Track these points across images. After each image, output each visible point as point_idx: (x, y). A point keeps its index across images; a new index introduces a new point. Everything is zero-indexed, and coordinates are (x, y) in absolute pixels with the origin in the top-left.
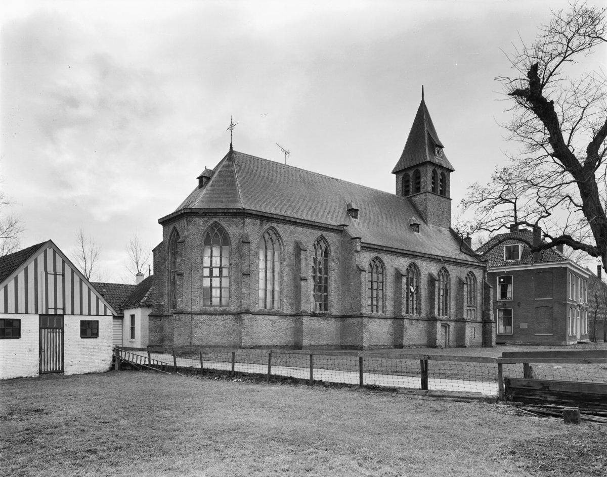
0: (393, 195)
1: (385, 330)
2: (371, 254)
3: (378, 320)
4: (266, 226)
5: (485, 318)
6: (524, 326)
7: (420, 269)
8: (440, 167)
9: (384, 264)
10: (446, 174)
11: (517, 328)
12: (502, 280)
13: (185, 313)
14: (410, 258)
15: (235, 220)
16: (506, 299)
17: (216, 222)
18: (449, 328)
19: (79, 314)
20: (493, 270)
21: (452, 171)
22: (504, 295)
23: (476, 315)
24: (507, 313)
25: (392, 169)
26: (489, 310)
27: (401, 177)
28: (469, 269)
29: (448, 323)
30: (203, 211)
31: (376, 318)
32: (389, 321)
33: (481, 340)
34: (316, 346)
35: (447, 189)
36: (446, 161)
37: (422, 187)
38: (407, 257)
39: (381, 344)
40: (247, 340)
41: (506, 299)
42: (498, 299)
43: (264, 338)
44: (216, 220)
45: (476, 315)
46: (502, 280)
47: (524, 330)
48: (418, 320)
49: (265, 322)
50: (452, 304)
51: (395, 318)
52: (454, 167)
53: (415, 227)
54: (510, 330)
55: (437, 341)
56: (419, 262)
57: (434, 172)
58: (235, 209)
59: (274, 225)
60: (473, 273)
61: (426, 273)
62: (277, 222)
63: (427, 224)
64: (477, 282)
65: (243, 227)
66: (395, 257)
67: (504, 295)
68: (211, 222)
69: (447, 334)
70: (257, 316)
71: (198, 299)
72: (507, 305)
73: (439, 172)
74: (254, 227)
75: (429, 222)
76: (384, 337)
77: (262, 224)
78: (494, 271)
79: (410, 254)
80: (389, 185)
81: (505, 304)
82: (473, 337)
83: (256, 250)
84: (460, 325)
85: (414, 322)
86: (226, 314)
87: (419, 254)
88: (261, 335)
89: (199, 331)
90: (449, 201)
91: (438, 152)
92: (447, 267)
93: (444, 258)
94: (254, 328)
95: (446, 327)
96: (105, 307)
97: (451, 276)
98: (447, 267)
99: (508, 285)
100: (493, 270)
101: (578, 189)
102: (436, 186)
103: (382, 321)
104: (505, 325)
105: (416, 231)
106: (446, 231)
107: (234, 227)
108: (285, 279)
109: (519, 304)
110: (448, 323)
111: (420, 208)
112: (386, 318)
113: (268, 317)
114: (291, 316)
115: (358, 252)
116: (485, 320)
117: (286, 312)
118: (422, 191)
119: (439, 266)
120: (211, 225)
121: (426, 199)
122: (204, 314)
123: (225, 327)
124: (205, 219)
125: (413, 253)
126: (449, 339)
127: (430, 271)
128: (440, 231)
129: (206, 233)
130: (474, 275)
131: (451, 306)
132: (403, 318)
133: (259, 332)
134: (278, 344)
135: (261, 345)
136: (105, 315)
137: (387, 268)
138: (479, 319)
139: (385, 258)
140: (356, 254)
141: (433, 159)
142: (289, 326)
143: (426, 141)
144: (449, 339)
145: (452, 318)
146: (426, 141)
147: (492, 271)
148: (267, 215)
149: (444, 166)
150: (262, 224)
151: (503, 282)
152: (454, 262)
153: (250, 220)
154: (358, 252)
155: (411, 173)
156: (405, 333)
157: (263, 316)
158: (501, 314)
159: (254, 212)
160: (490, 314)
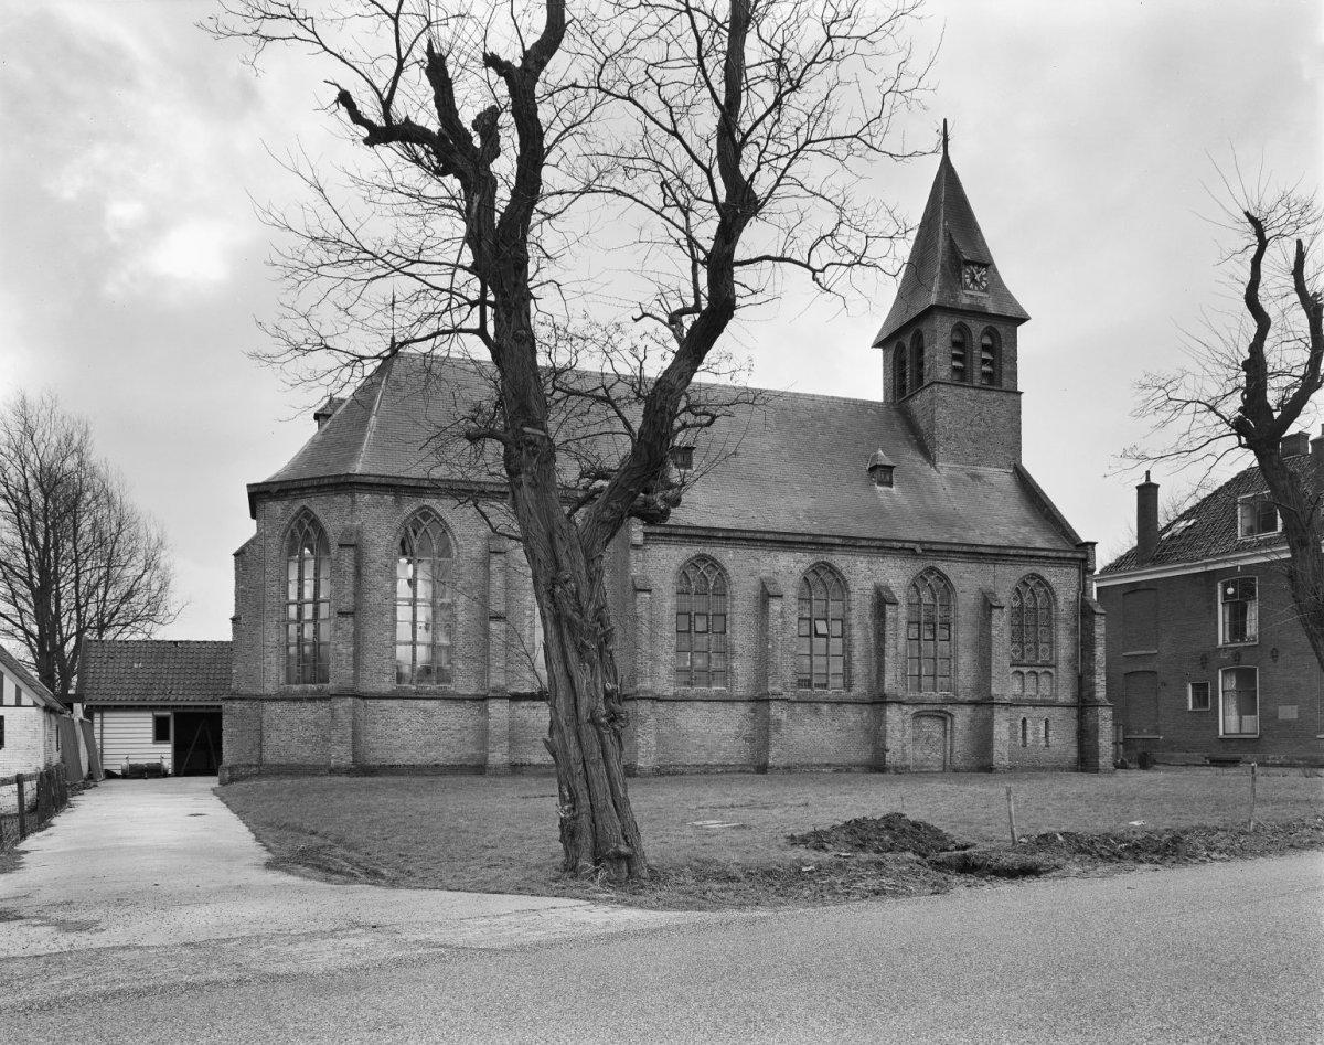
0: (863, 406)
1: (730, 729)
2: (684, 550)
3: (705, 706)
4: (410, 506)
5: (1085, 694)
6: (1288, 713)
7: (847, 576)
8: (979, 313)
9: (724, 570)
10: (1002, 329)
11: (1268, 720)
12: (1230, 591)
13: (242, 699)
14: (812, 552)
15: (338, 499)
16: (1243, 640)
17: (304, 508)
18: (952, 723)
19: (14, 703)
20: (1206, 564)
21: (1023, 319)
22: (1237, 629)
23: (1055, 685)
24: (1245, 677)
25: (872, 337)
26: (1092, 673)
27: (891, 352)
28: (1026, 570)
29: (949, 708)
30: (277, 488)
31: (698, 700)
32: (742, 708)
33: (1073, 753)
34: (544, 765)
35: (1007, 368)
36: (1006, 296)
37: (926, 374)
38: (799, 550)
39: (714, 761)
40: (342, 754)
41: (1243, 640)
42: (1221, 642)
43: (403, 747)
44: (304, 502)
45: (1055, 685)
46: (1230, 591)
47: (1288, 723)
48: (839, 703)
49: (406, 714)
50: (961, 661)
51: (757, 700)
52: (1028, 308)
53: (878, 474)
54: (1251, 724)
55: (888, 755)
56: (840, 560)
57: (961, 329)
58: (331, 476)
59: (430, 502)
60: (1041, 578)
61: (869, 585)
62: (438, 496)
63: (929, 456)
64: (1056, 600)
65: (352, 512)
66: (760, 553)
67: (1237, 629)
68: (296, 508)
69: (948, 736)
70: (384, 702)
71: (274, 669)
72: (1244, 659)
73: (977, 327)
74: (380, 511)
75: (940, 452)
76: (724, 745)
77: (398, 502)
78: (1209, 568)
79: (810, 543)
80: (866, 379)
81: (1237, 656)
82: (1043, 743)
83: (385, 560)
84: (982, 712)
85: (825, 707)
86: (320, 699)
87: (837, 541)
88: (397, 743)
89: (274, 734)
90: (1012, 397)
91: (973, 280)
92: (942, 566)
93: (927, 546)
94: (379, 728)
95: (944, 719)
96: (18, 691)
97: (959, 589)
98: (942, 566)
99: (1249, 603)
100: (1206, 564)
101: (538, 360)
102: (968, 366)
103: (720, 707)
104: (1241, 713)
105: (881, 483)
106: (1002, 478)
107: (335, 515)
108: (460, 618)
109: (1275, 654)
110: (949, 708)
111: (923, 425)
112: (732, 701)
113: (414, 702)
114: (970, 703)
115: (636, 547)
116: (1084, 701)
117: (462, 692)
118: (926, 382)
119: (914, 567)
120: (298, 514)
121: (931, 402)
122: (283, 699)
123: (317, 725)
124: (286, 503)
125: (816, 540)
126: (951, 751)
127: (882, 581)
128: (976, 477)
129: (289, 532)
130: (1047, 583)
131: (961, 667)
132: (768, 700)
133: (391, 736)
134: (441, 761)
135: (396, 762)
136: (18, 704)
137: (734, 579)
138: (1065, 695)
139: (728, 557)
140: (633, 553)
141: (955, 297)
142: (470, 723)
143: (939, 256)
144: (951, 751)
145: (961, 697)
146: (939, 256)
147: (1204, 569)
148: (405, 483)
149: (992, 310)
150: (398, 502)
151: (1234, 595)
152: (965, 553)
153: (367, 496)
154: (636, 547)
155: (907, 341)
156: (775, 736)
157: (401, 702)
158: (1232, 683)
159: (372, 480)
160: (1093, 685)
